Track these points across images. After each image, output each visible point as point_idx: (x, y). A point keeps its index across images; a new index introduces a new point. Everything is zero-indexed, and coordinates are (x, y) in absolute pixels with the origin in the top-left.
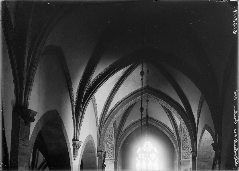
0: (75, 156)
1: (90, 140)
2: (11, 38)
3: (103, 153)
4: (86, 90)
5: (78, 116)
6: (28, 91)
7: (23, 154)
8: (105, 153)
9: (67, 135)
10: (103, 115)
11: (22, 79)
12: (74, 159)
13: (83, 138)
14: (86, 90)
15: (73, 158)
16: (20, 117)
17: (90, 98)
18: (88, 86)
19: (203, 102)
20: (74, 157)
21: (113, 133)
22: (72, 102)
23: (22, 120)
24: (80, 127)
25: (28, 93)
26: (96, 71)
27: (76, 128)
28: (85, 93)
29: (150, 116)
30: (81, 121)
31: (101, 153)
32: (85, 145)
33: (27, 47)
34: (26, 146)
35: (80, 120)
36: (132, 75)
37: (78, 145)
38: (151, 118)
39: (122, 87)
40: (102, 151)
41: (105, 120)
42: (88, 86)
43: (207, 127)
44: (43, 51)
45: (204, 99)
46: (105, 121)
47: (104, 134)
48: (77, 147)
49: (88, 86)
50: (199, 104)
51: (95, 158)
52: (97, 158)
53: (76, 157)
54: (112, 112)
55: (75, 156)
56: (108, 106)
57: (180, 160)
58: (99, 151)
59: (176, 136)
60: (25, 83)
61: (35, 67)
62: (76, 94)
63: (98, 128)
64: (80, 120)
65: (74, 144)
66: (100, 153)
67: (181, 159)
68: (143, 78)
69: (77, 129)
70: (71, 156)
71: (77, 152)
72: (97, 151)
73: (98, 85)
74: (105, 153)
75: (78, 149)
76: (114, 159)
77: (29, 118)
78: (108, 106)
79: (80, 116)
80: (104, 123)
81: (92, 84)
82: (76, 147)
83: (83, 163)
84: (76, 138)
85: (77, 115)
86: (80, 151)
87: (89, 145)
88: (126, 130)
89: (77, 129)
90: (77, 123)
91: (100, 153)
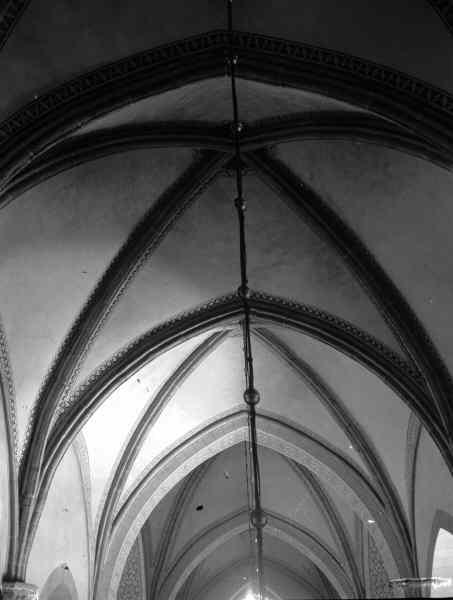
5: (26, 493)
10: (106, 508)
14: (58, 411)
19: (419, 433)
20: (84, 89)
21: (142, 564)
24: (30, 532)
28: (54, 420)
39: (117, 309)
42: (67, 399)
45: (420, 429)
54: (138, 488)
63: (93, 544)
68: (256, 386)
69: (21, 541)
78: (127, 468)
79: (34, 496)
81: (78, 394)
84: (13, 573)
85: (23, 492)
89: (21, 541)
90: (21, 502)
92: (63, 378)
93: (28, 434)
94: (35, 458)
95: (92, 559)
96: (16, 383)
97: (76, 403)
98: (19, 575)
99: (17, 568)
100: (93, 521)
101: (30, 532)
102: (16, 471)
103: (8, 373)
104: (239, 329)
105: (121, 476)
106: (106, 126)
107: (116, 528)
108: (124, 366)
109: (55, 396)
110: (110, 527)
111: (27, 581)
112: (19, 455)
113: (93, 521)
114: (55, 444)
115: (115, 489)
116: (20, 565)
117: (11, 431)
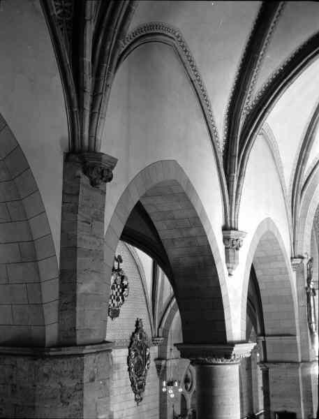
0: (231, 265)
1: (269, 233)
2: (57, 10)
3: (305, 262)
5: (230, 172)
6: (97, 115)
7: (89, 253)
9: (206, 217)
10: (295, 179)
11: (80, 90)
12: (230, 275)
13: (249, 220)
15: (227, 275)
16: (80, 172)
17: (254, 131)
18: (249, 102)
20: (228, 268)
22: (211, 133)
23: (85, 180)
24: (237, 197)
25: (96, 120)
26: (263, 68)
30: (238, 186)
31: (302, 262)
32: (257, 242)
33: (88, 23)
34: (98, 238)
35: (235, 183)
37: (237, 240)
40: (303, 258)
41: (303, 184)
42: (250, 104)
48: (233, 245)
49: (249, 102)
51: (287, 273)
52: (293, 275)
53: (232, 268)
55: (231, 265)
58: (295, 258)
60: (88, 100)
61: (109, 63)
64: (235, 183)
65: (226, 239)
66: (299, 261)
70: (221, 267)
71: (235, 257)
72: (292, 258)
73: (277, 90)
75: (237, 249)
77: (98, 171)
82: (231, 245)
83: (258, 273)
86: (244, 257)
87: (267, 241)
90: (227, 180)
91: (299, 262)
92: (245, 89)
93: (226, 133)
94: (232, 150)
95: (290, 213)
96: (210, 98)
97: (257, 106)
98: (233, 226)
99: (231, 221)
100: (288, 188)
101: (237, 197)
102: (221, 160)
103: (201, 86)
104: (181, 341)
105: (303, 157)
106: (91, 38)
107: (305, 192)
108: (248, 132)
109: (241, 102)
110: (299, 196)
111: (239, 229)
112: (221, 147)
113: (288, 188)
114: (246, 138)
115: (300, 166)
116: (233, 219)
117: (212, 132)
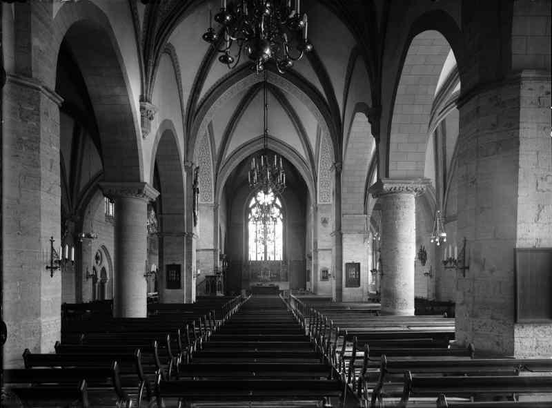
4: (158, 25)
8: (198, 168)
15: (141, 134)
20: (143, 132)
27: (144, 81)
29: (270, 133)
36: (330, 219)
38: (272, 139)
43: (360, 107)
44: (300, 313)
46: (197, 113)
47: (195, 134)
50: (346, 79)
55: (145, 129)
56: (169, 30)
57: (316, 203)
59: (310, 165)
62: (187, 100)
67: (318, 202)
74: (198, 168)
76: (213, 202)
80: (196, 115)
88: (205, 100)
89: (147, 83)
